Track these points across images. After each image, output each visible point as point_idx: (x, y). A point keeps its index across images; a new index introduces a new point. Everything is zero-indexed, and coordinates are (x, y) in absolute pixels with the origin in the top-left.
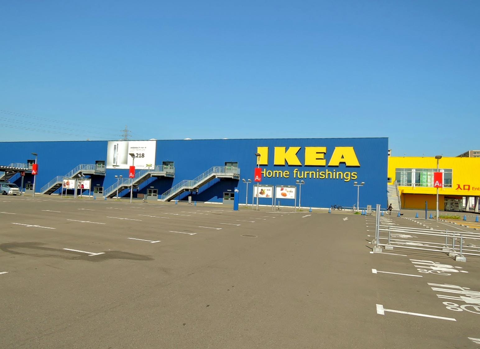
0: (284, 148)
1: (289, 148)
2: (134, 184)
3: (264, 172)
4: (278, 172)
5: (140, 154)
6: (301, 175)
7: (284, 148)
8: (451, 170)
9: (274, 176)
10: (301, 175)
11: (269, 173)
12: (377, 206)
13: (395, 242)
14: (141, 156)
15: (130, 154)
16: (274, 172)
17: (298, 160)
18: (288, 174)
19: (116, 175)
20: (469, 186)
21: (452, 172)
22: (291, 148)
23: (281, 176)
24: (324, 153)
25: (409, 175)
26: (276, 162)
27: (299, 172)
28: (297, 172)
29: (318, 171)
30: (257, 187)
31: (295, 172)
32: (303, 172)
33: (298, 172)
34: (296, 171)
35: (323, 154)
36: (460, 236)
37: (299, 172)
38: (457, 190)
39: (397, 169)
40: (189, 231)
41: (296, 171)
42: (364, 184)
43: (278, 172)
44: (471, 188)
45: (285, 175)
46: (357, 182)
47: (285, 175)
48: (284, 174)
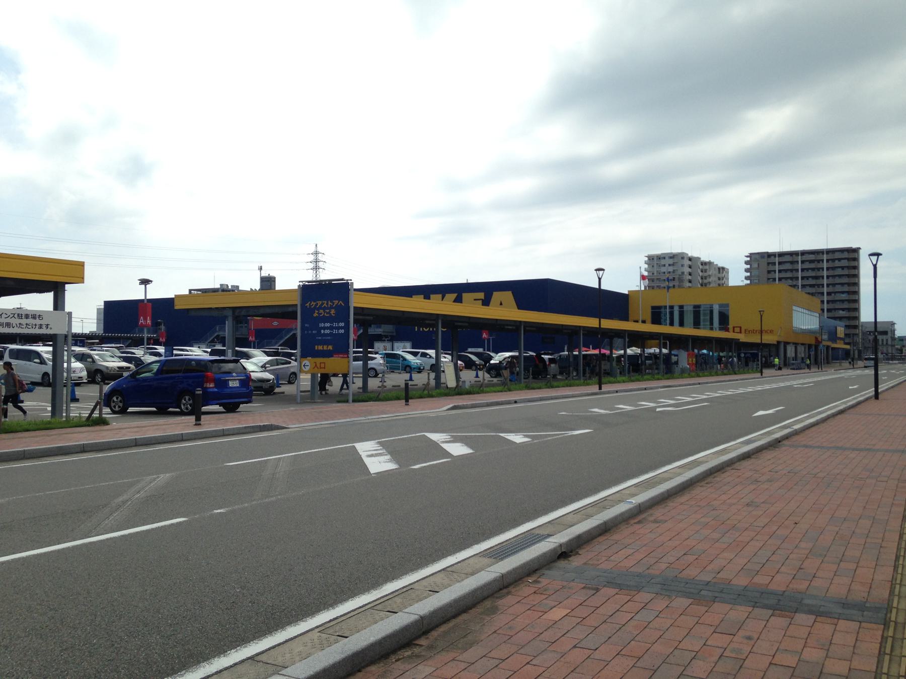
1: (445, 295)
2: (46, 358)
8: (727, 305)
12: (371, 333)
15: (433, 358)
17: (492, 299)
19: (415, 328)
20: (740, 328)
21: (728, 307)
22: (447, 296)
24: (482, 299)
25: (672, 314)
29: (66, 350)
30: (147, 298)
35: (481, 301)
36: (331, 328)
39: (653, 308)
42: (418, 328)
44: (743, 331)
46: (416, 327)
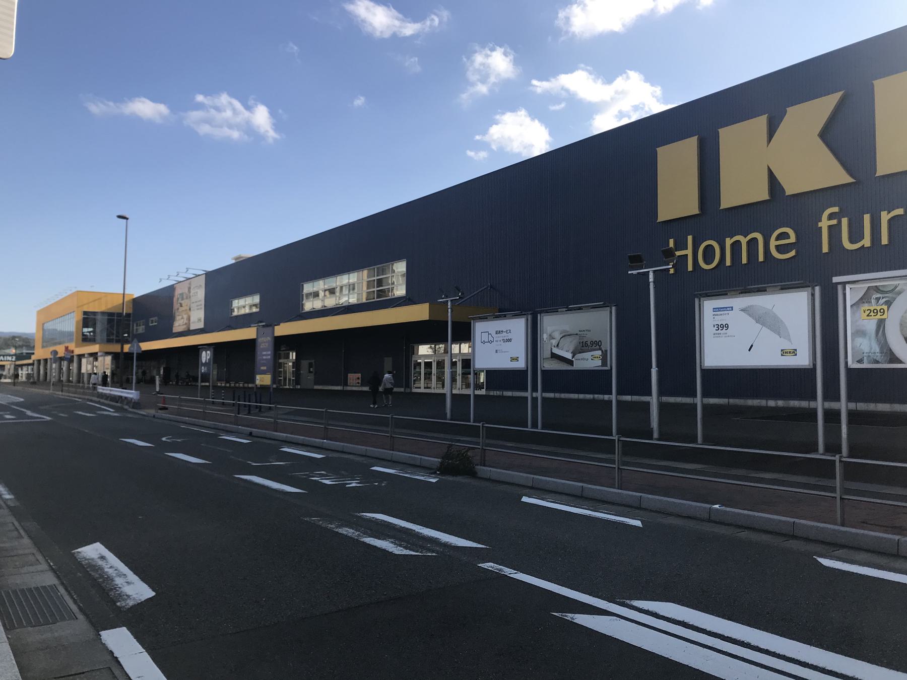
0: (865, 246)
3: (689, 252)
4: (744, 241)
5: (582, 342)
6: (856, 235)
7: (761, 122)
9: (728, 263)
10: (856, 235)
11: (709, 254)
13: (219, 409)
14: (584, 345)
16: (729, 242)
18: (793, 239)
23: (761, 258)
26: (729, 199)
27: (845, 221)
28: (834, 222)
31: (825, 224)
32: (885, 241)
33: (840, 222)
34: (831, 217)
37: (845, 221)
38: (143, 675)
40: (197, 425)
41: (831, 217)
43: (744, 241)
45: (779, 248)
47: (779, 248)
48: (773, 243)
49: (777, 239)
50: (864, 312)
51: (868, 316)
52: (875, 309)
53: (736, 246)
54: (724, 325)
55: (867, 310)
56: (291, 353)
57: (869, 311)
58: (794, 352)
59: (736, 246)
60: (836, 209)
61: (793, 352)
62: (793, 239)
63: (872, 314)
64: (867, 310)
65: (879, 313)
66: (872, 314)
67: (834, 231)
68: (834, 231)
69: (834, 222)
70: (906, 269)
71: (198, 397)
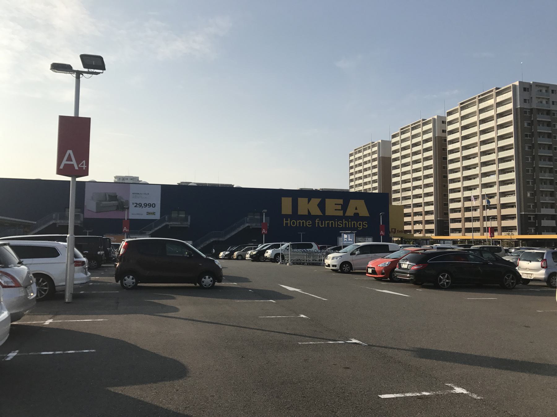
3: (289, 222)
4: (301, 222)
6: (322, 224)
10: (322, 224)
18: (311, 223)
27: (320, 222)
28: (318, 221)
31: (317, 221)
34: (318, 220)
37: (320, 222)
41: (318, 220)
43: (301, 222)
48: (307, 223)
49: (308, 223)
50: (133, 204)
51: (135, 207)
52: (145, 203)
53: (300, 222)
54: (152, 204)
55: (135, 203)
56: (394, 203)
57: (136, 204)
58: (154, 213)
59: (300, 222)
60: (319, 219)
61: (153, 213)
62: (311, 223)
63: (138, 206)
64: (135, 203)
65: (148, 206)
66: (138, 206)
67: (318, 223)
68: (318, 223)
69: (318, 221)
70: (554, 375)
71: (87, 235)
